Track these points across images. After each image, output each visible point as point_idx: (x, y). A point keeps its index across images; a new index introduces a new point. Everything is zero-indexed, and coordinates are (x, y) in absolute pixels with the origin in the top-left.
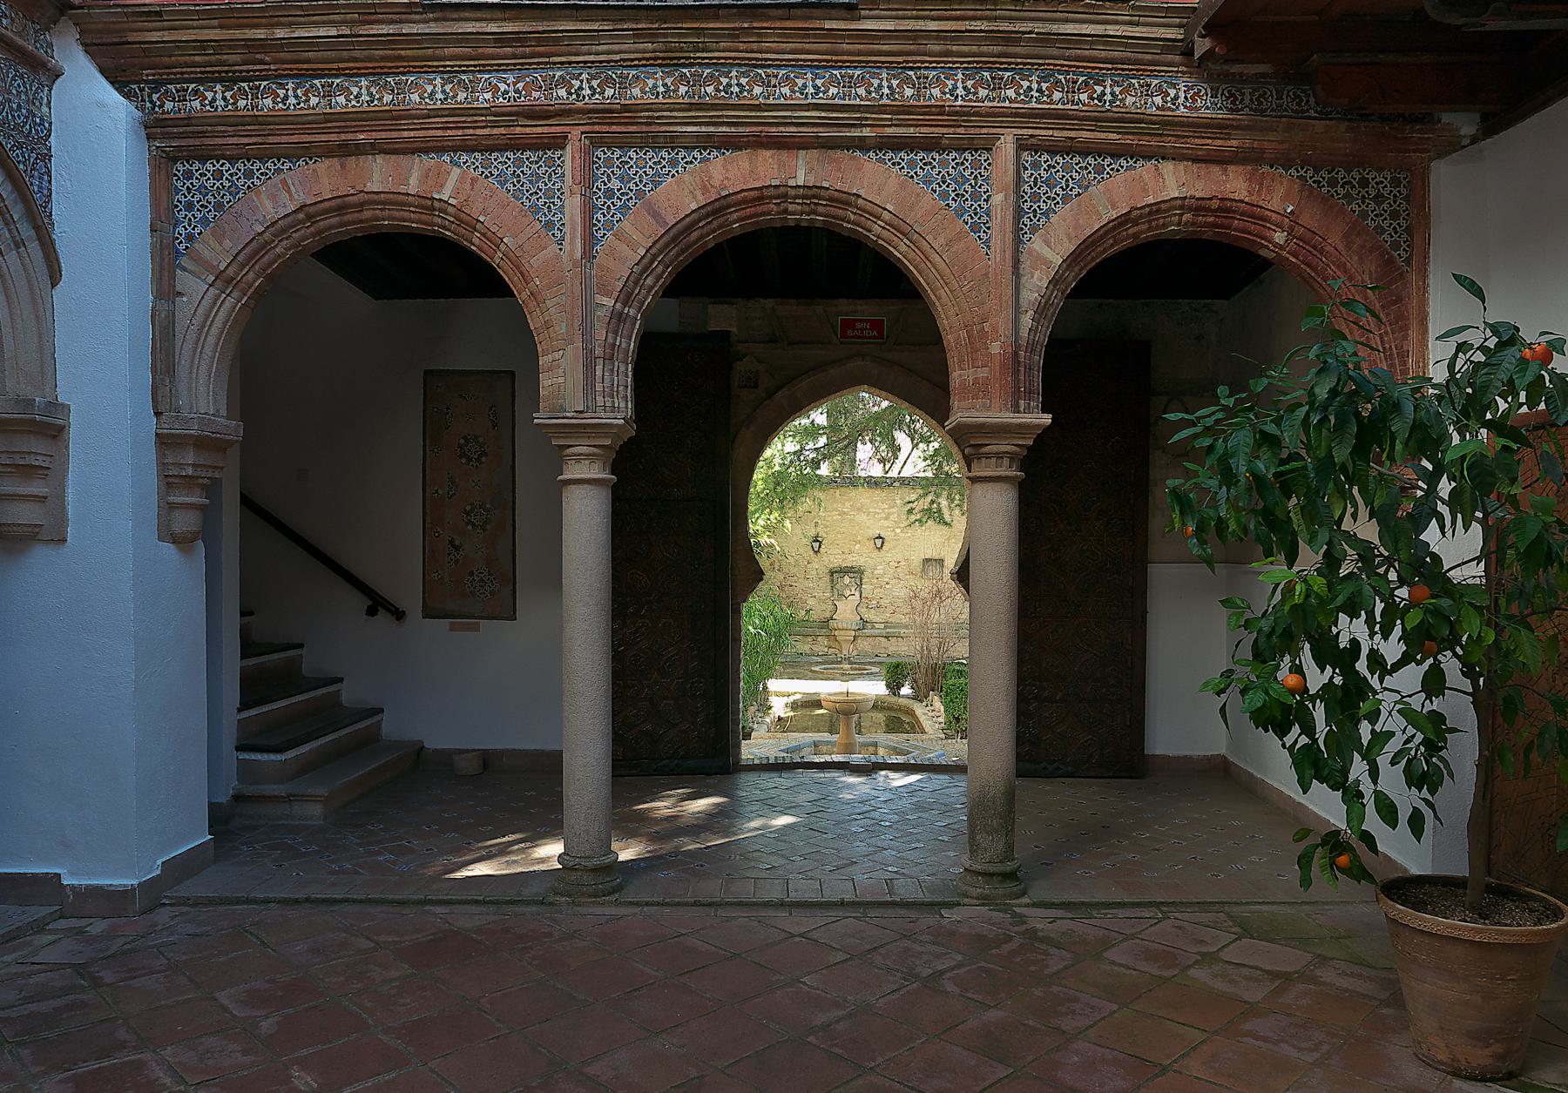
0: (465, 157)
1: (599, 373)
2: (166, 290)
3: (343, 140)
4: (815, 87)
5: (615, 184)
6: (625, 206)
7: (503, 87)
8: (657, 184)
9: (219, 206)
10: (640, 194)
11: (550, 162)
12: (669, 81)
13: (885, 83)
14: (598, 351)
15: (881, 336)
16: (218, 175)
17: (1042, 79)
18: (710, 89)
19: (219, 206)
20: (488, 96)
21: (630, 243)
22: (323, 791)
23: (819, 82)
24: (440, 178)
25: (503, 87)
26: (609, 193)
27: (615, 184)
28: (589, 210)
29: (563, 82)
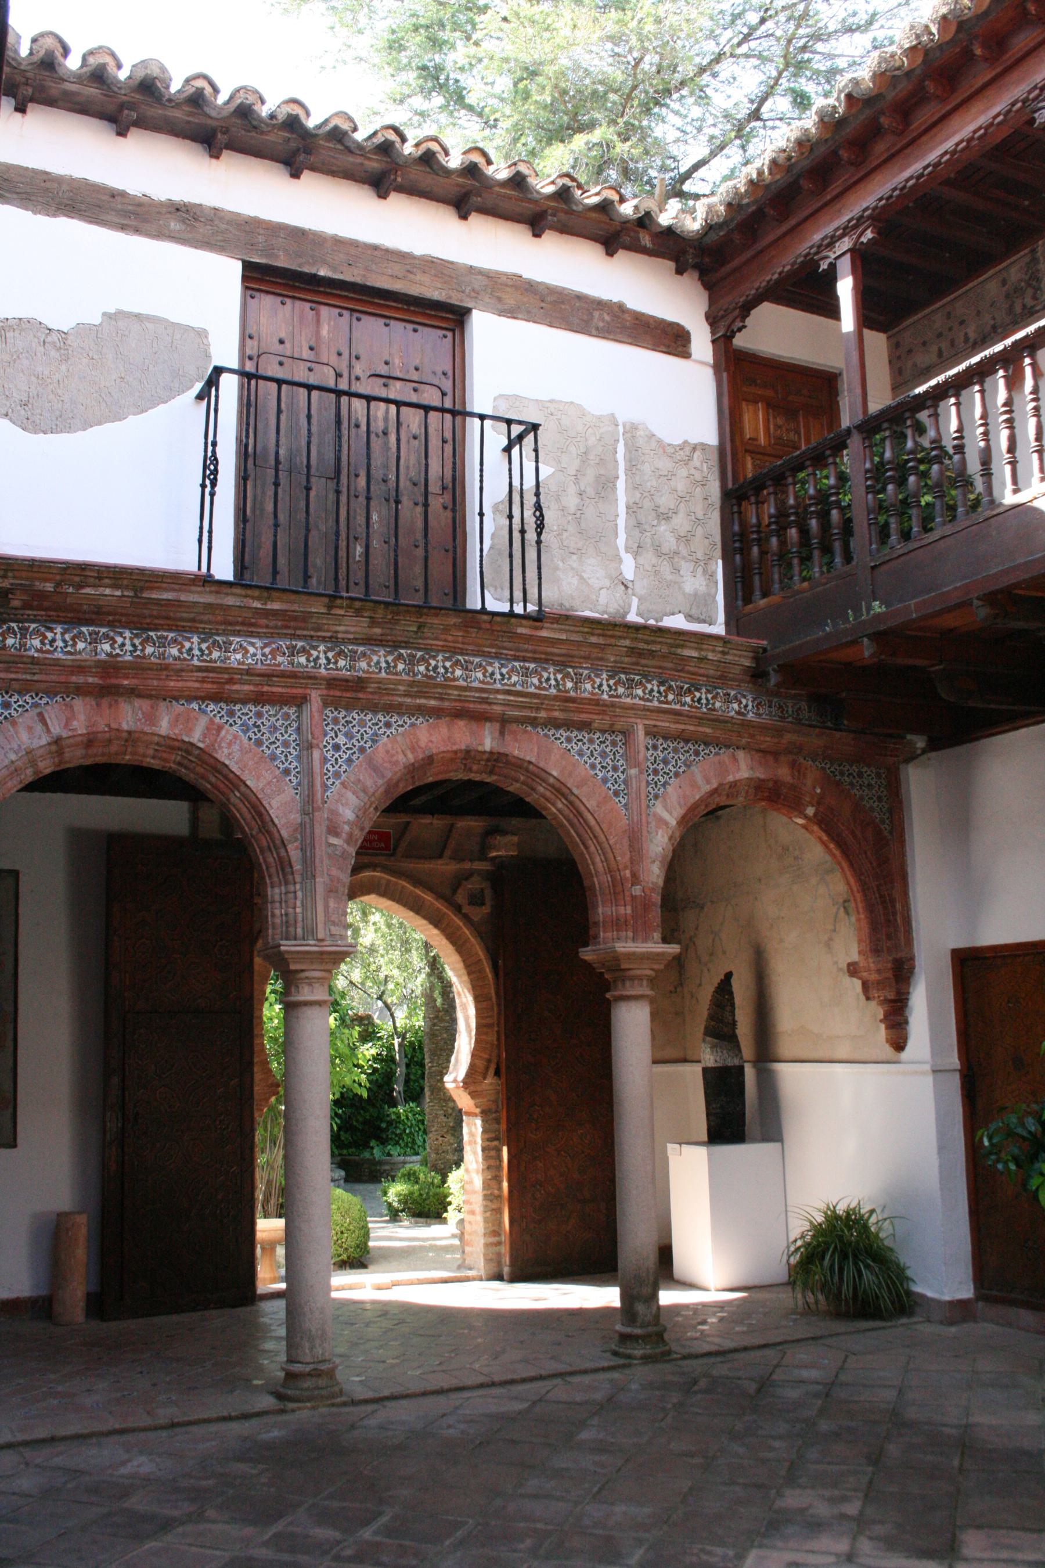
0: (212, 707)
5: (341, 740)
7: (252, 650)
8: (374, 741)
15: (387, 848)
18: (422, 668)
20: (239, 656)
23: (504, 671)
25: (252, 650)
26: (337, 747)
27: (341, 740)
29: (303, 650)
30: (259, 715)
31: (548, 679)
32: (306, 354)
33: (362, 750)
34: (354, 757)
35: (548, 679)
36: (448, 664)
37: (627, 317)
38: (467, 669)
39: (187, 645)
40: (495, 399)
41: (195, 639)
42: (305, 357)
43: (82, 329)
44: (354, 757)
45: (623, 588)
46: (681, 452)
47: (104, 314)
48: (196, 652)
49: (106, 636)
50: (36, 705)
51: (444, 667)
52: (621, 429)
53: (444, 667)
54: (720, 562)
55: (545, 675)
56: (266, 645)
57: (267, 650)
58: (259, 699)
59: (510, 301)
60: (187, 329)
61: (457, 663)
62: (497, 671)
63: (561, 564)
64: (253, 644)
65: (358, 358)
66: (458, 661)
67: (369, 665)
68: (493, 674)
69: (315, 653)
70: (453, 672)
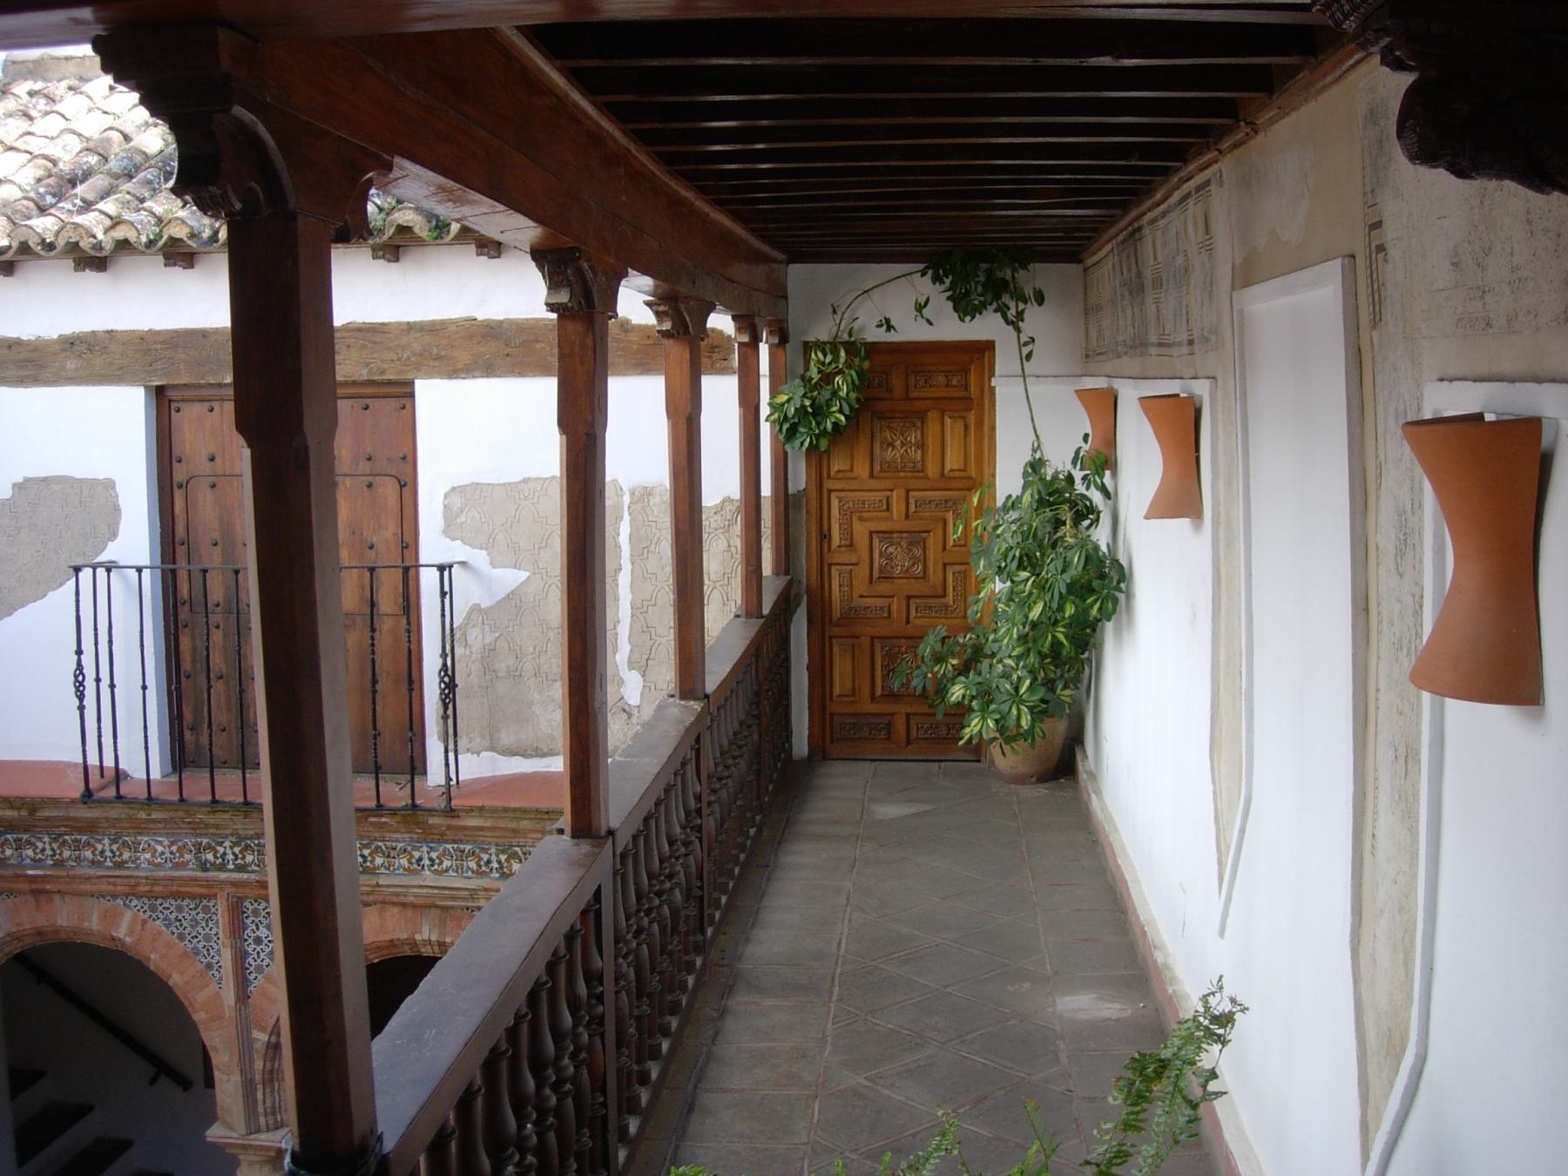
0: (135, 902)
1: (260, 1095)
3: (39, 891)
4: (431, 860)
7: (160, 849)
11: (206, 909)
13: (494, 858)
14: (258, 1077)
17: (114, 841)
20: (148, 856)
22: (156, 774)
23: (434, 855)
24: (112, 917)
25: (160, 849)
26: (258, 941)
28: (240, 958)
29: (209, 847)
30: (180, 909)
31: (489, 862)
35: (489, 862)
37: (633, 337)
39: (100, 847)
40: (446, 496)
41: (106, 841)
45: (625, 716)
46: (718, 517)
47: (14, 485)
48: (108, 854)
49: (29, 842)
52: (626, 499)
54: (837, 690)
55: (485, 857)
56: (172, 843)
57: (174, 848)
58: (177, 895)
59: (463, 357)
60: (93, 483)
62: (426, 856)
63: (537, 696)
64: (160, 843)
66: (378, 847)
68: (420, 859)
69: (221, 850)
70: (372, 861)
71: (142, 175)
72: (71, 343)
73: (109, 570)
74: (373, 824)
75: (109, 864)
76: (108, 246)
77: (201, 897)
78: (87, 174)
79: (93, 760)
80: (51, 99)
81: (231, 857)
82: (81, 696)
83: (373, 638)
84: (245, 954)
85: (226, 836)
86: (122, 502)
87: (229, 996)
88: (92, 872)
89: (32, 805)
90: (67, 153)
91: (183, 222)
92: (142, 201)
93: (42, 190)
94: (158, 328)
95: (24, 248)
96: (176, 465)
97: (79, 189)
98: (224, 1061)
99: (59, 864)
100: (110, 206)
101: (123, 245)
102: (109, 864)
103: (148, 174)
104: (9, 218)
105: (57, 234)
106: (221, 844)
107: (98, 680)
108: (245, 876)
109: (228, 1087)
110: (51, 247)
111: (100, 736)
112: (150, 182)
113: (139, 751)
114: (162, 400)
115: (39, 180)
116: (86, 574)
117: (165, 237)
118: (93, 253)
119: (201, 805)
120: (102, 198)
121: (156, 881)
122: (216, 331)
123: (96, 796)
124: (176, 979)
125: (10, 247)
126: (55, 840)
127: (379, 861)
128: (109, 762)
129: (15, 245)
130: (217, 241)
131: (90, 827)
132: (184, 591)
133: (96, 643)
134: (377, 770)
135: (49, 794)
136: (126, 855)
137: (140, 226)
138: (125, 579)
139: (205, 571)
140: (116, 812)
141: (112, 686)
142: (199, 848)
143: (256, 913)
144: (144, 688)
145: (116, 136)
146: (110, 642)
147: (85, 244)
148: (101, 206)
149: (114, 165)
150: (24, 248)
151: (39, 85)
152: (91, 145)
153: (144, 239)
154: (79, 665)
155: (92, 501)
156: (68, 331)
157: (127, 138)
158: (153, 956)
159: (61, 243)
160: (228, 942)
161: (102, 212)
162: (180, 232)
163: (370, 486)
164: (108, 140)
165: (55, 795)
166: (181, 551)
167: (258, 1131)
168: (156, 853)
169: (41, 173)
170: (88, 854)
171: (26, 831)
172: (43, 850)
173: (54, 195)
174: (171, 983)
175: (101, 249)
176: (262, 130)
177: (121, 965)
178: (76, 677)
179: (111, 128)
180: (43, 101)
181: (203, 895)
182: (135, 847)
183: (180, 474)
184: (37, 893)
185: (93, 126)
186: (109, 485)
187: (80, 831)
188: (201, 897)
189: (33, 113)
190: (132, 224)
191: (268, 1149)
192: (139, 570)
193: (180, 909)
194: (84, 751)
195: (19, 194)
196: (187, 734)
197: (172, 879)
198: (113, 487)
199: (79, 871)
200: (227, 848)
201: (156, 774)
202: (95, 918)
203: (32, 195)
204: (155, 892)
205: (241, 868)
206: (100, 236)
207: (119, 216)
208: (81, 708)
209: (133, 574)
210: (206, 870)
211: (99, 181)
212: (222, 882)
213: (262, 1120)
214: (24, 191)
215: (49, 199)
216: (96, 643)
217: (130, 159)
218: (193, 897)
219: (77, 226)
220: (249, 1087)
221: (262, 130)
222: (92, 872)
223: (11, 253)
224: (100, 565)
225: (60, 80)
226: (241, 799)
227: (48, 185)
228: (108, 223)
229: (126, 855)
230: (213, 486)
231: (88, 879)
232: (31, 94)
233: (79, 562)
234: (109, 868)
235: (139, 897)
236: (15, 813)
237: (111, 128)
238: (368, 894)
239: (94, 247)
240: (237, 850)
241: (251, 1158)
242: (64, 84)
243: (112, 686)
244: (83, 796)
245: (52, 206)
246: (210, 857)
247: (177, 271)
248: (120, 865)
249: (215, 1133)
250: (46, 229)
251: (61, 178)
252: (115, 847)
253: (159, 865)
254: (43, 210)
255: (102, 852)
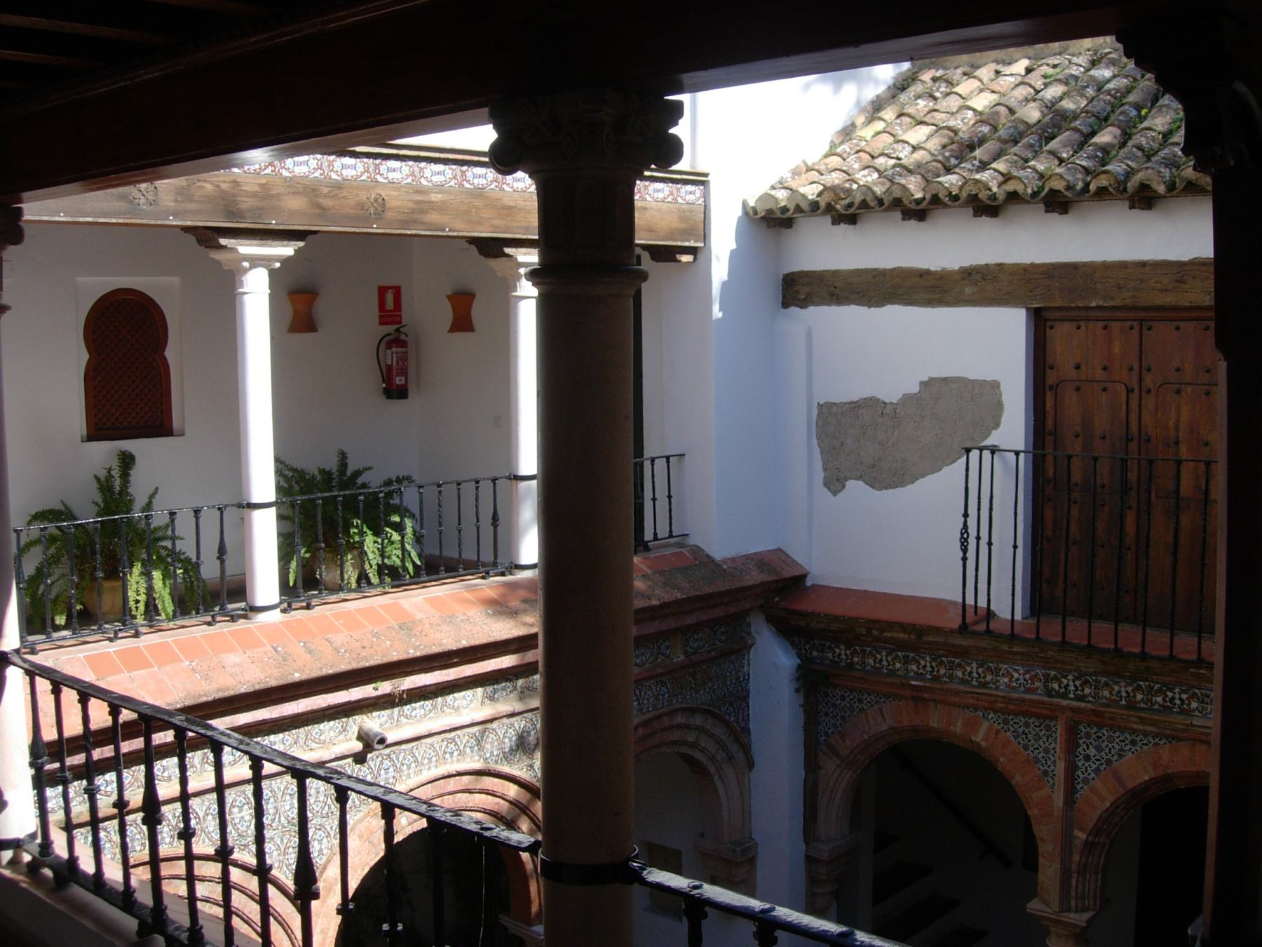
0: (992, 715)
1: (1074, 882)
2: (811, 765)
3: (918, 698)
5: (1092, 752)
6: (1097, 769)
7: (1016, 675)
8: (1121, 756)
9: (843, 718)
10: (1109, 762)
11: (1048, 728)
12: (1130, 689)
14: (1074, 867)
16: (843, 698)
17: (980, 666)
18: (1159, 699)
19: (843, 718)
20: (1006, 680)
21: (1099, 796)
22: (1018, 616)
25: (1016, 675)
26: (1087, 758)
27: (1092, 752)
28: (1071, 769)
29: (1055, 679)
30: (1027, 725)
32: (1100, 374)
33: (1109, 762)
34: (1102, 768)
36: (1184, 696)
38: (1203, 702)
39: (969, 669)
41: (974, 665)
42: (1098, 377)
43: (907, 399)
44: (1102, 768)
47: (921, 383)
48: (975, 675)
50: (877, 702)
51: (1181, 699)
53: (1181, 699)
56: (1027, 672)
57: (1027, 676)
61: (1194, 696)
64: (1017, 671)
65: (1149, 370)
66: (1194, 694)
67: (1111, 693)
70: (1189, 705)
71: (1025, 141)
72: (969, 273)
73: (993, 453)
74: (1192, 674)
75: (974, 683)
76: (1001, 197)
77: (1046, 717)
78: (982, 141)
79: (970, 600)
80: (950, 83)
81: (1072, 688)
82: (965, 551)
83: (1205, 520)
84: (1075, 768)
85: (1070, 671)
86: (1004, 398)
87: (1059, 800)
88: (961, 688)
89: (920, 631)
90: (964, 123)
91: (1061, 177)
92: (1027, 161)
93: (947, 154)
94: (1038, 261)
95: (935, 200)
96: (1048, 371)
97: (977, 153)
98: (1047, 848)
99: (936, 679)
100: (1001, 165)
101: (1013, 197)
102: (974, 683)
103: (1031, 139)
104: (923, 176)
105: (961, 188)
106: (1065, 677)
107: (978, 538)
108: (1083, 705)
109: (1049, 872)
110: (955, 198)
111: (976, 582)
112: (1032, 146)
113: (1005, 596)
114: (1040, 323)
115: (944, 147)
116: (974, 454)
117: (1046, 190)
118: (989, 202)
119: (1053, 644)
120: (995, 160)
121: (1009, 700)
122: (1196, 264)
123: (970, 629)
124: (1018, 779)
125: (924, 199)
126: (934, 660)
127: (1194, 705)
128: (982, 603)
129: (928, 196)
130: (1088, 191)
131: (963, 653)
132: (1132, 476)
133: (979, 509)
134: (1172, 629)
135: (933, 624)
136: (989, 678)
137: (1026, 181)
138: (1004, 461)
139: (1070, 457)
140: (984, 643)
141: (990, 544)
142: (1046, 676)
143: (1088, 735)
144: (1015, 547)
145: (1002, 109)
146: (991, 509)
147: (983, 195)
148: (994, 165)
149: (1002, 133)
150: (935, 200)
151: (939, 73)
152: (984, 117)
153: (1029, 191)
154: (965, 525)
155: (981, 399)
156: (966, 264)
157: (1012, 111)
158: (1001, 759)
159: (964, 195)
160: (1062, 756)
161: (995, 170)
162: (1058, 185)
163: (1207, 393)
164: (997, 113)
165: (940, 625)
166: (1049, 440)
167: (1069, 910)
168: (1013, 679)
169: (945, 140)
170: (960, 674)
171: (913, 651)
172: (925, 667)
173: (957, 158)
174: (1013, 782)
175: (996, 199)
176: (1252, 100)
177: (975, 765)
178: (962, 534)
179: (999, 104)
180: (944, 85)
181: (1046, 715)
182: (996, 672)
183: (1051, 379)
184: (915, 698)
185: (982, 102)
186: (995, 385)
187: (955, 655)
188: (1046, 717)
189: (938, 94)
190: (1020, 179)
191: (1075, 926)
192: (1017, 453)
193: (1027, 725)
194: (964, 593)
195: (929, 158)
196: (1045, 586)
197: (1024, 700)
198: (998, 387)
199: (952, 686)
200: (1070, 681)
201: (1018, 616)
202: (959, 724)
203: (940, 158)
204: (1010, 709)
205: (1081, 698)
206: (995, 189)
207: (1009, 173)
208: (964, 559)
209: (1012, 456)
210: (1051, 696)
211: (991, 146)
212: (1064, 708)
213: (1073, 903)
214: (933, 155)
215: (953, 161)
216: (979, 509)
217: (1016, 128)
218: (1038, 716)
219: (977, 181)
220: (1065, 875)
221: (1252, 100)
222: (961, 688)
223: (925, 203)
224: (986, 448)
225: (956, 68)
226: (1085, 643)
227: (952, 150)
228: (1001, 178)
229: (989, 678)
230: (1078, 389)
231: (957, 693)
232: (934, 80)
233: (968, 445)
234: (975, 686)
235: (995, 711)
236: (906, 636)
237: (999, 104)
238: (1182, 731)
239: (989, 198)
240: (1078, 683)
241: (1060, 931)
242: (959, 71)
243: (990, 544)
244: (960, 627)
245: (956, 166)
246: (1056, 686)
247: (1054, 216)
248: (984, 685)
249: (1034, 906)
250: (952, 184)
251: (962, 144)
252: (980, 670)
253: (1014, 688)
254: (948, 170)
255: (971, 673)
